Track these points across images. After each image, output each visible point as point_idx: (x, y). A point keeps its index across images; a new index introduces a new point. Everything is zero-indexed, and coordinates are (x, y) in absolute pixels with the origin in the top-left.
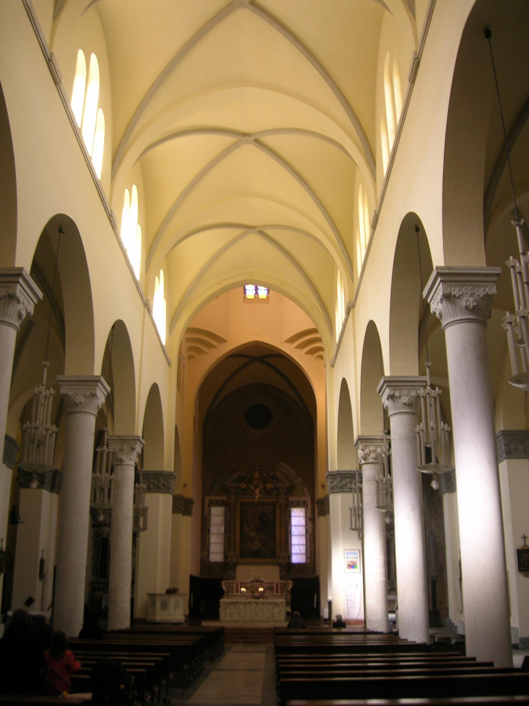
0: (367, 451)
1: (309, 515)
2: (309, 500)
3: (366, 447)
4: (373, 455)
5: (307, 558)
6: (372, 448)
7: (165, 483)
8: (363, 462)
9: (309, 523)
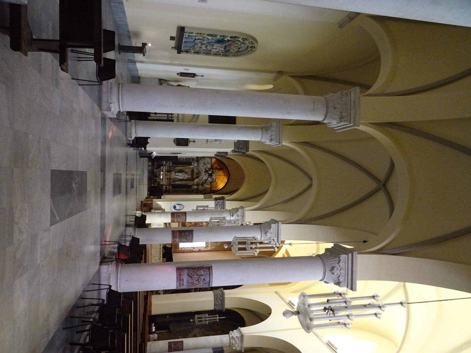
0: (236, 339)
1: (202, 249)
2: (209, 249)
3: (238, 338)
4: (234, 342)
5: (182, 248)
6: (237, 342)
7: (219, 204)
8: (231, 336)
9: (198, 249)
